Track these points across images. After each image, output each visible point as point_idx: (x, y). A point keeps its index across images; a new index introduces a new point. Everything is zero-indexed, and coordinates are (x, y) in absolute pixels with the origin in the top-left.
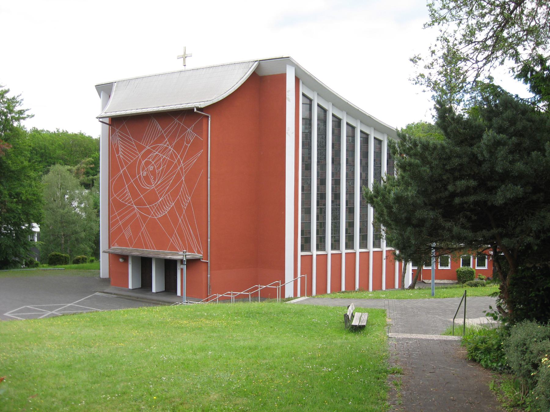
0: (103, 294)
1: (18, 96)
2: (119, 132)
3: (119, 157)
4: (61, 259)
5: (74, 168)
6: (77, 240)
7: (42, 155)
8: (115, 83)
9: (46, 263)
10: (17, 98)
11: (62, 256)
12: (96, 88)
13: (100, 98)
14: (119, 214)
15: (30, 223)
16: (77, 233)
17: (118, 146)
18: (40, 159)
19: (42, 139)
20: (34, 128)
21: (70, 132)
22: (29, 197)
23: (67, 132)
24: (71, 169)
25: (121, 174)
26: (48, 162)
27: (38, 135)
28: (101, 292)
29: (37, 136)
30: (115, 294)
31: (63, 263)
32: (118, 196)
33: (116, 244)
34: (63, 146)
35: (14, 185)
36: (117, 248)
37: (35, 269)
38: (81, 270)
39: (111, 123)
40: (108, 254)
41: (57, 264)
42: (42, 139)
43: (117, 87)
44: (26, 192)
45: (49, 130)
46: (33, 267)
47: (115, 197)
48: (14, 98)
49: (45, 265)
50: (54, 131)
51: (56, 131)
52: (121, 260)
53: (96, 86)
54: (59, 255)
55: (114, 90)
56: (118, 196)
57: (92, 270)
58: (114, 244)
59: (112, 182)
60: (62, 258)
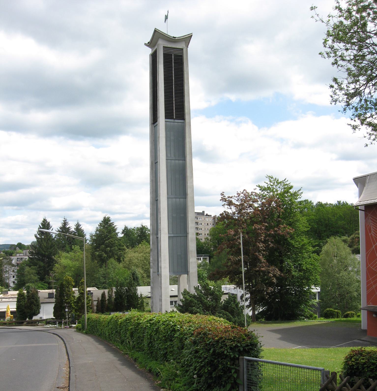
0: (361, 341)
1: (298, 191)
2: (371, 216)
3: (371, 235)
4: (334, 314)
5: (349, 239)
6: (351, 298)
7: (327, 225)
8: (368, 177)
9: (323, 317)
10: (297, 192)
11: (335, 312)
12: (354, 181)
13: (358, 187)
14: (373, 280)
15: (309, 286)
16: (350, 292)
17: (370, 227)
18: (325, 229)
19: (325, 212)
20: (319, 202)
21: (349, 203)
22: (308, 266)
23: (347, 204)
24: (347, 239)
25: (373, 249)
26: (331, 231)
27: (322, 208)
28: (359, 340)
29: (321, 209)
30: (369, 342)
31: (335, 317)
32: (371, 266)
33: (371, 303)
34: (344, 217)
35: (292, 264)
36: (371, 306)
37: (314, 320)
38: (348, 323)
39: (365, 209)
40: (366, 311)
41: (330, 318)
42: (325, 212)
43: (369, 179)
44: (306, 263)
45: (332, 203)
46: (312, 319)
47: (369, 266)
48: (295, 193)
49: (322, 318)
50: (336, 204)
51: (337, 203)
52: (374, 315)
53: (353, 179)
54: (332, 311)
55: (367, 182)
56: (371, 266)
57: (356, 323)
58: (370, 303)
59: (368, 254)
60: (335, 313)
